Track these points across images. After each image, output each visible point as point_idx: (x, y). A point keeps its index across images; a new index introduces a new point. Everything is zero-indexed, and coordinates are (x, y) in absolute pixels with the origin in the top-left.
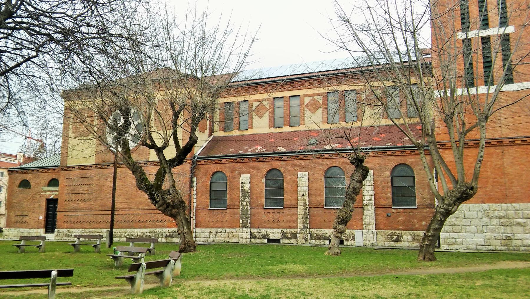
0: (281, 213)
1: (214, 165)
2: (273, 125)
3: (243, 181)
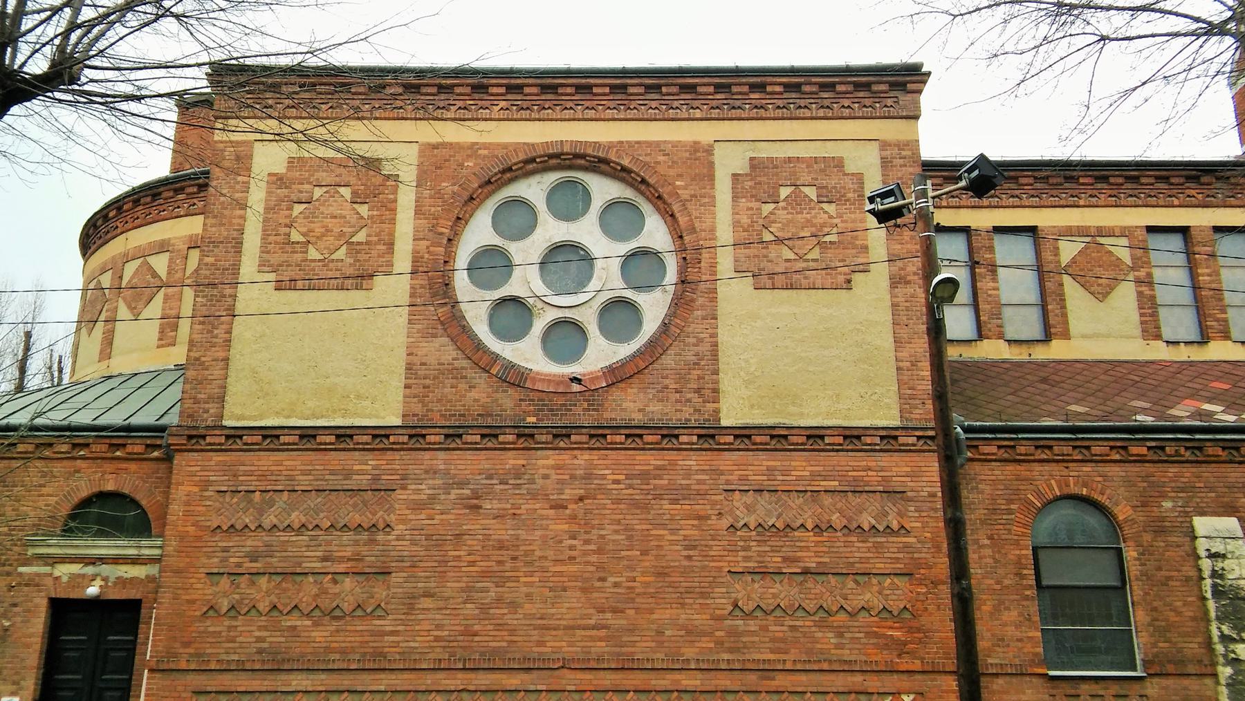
1: (1047, 467)
2: (1151, 330)
3: (1218, 547)
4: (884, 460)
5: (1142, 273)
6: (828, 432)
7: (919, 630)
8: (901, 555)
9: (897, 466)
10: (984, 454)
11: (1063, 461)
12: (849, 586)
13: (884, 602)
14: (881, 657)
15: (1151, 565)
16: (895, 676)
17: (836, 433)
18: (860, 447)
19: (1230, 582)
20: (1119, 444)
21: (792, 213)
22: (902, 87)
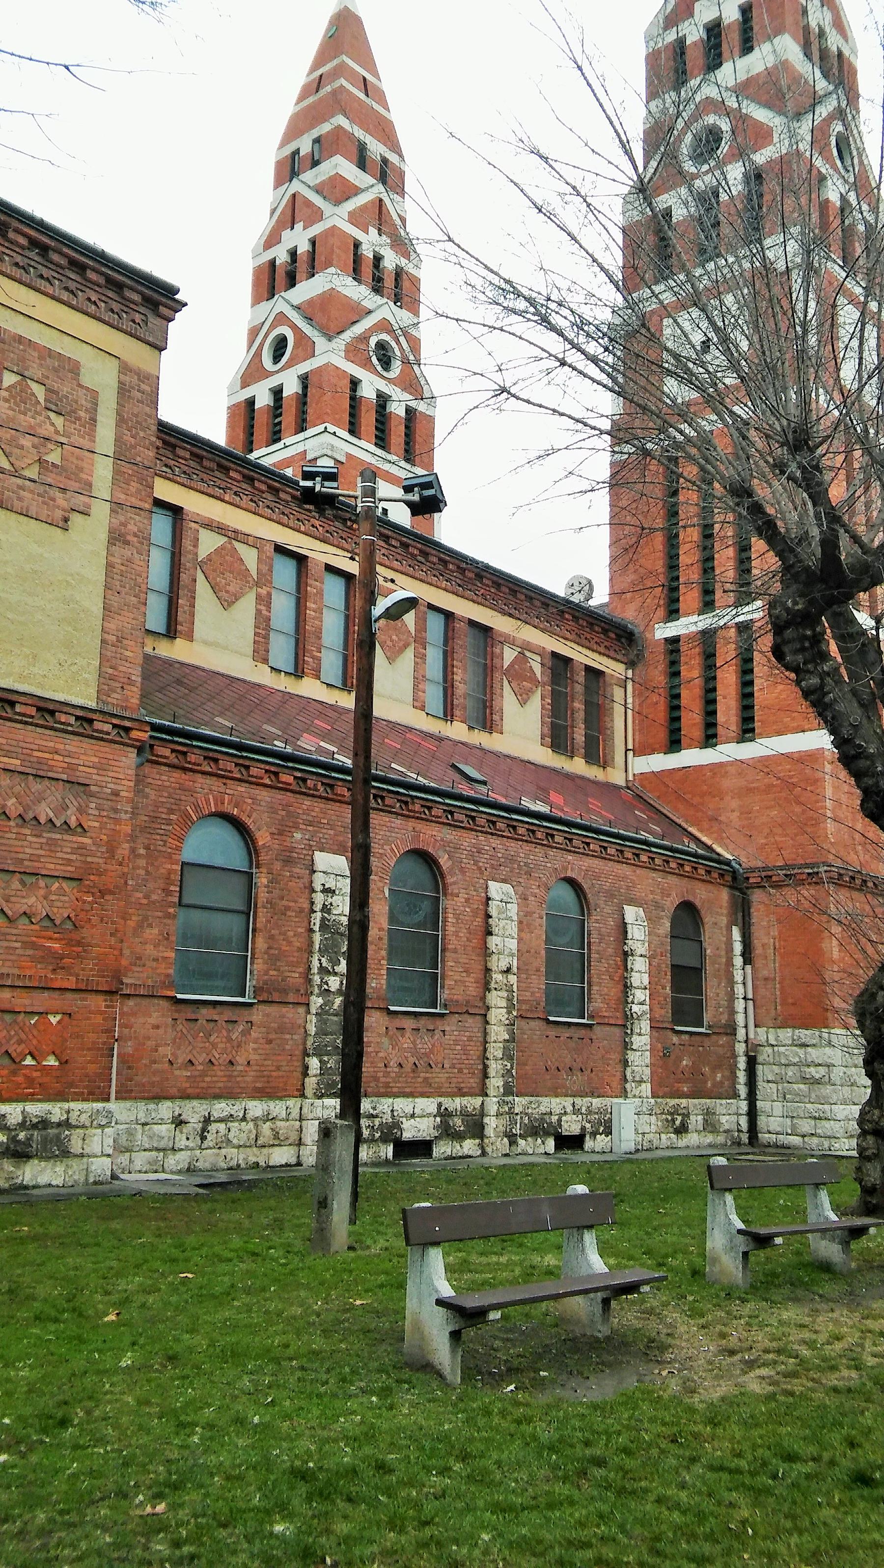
0: (438, 1034)
2: (261, 653)
3: (331, 884)
4: (73, 744)
5: (263, 591)
6: (22, 699)
7: (79, 943)
8: (74, 857)
9: (85, 754)
10: (157, 756)
11: (223, 777)
12: (14, 887)
13: (48, 908)
14: (42, 971)
15: (276, 892)
16: (46, 994)
17: (30, 702)
18: (51, 724)
19: (334, 917)
20: (273, 769)
21: (14, 410)
22: (153, 305)
